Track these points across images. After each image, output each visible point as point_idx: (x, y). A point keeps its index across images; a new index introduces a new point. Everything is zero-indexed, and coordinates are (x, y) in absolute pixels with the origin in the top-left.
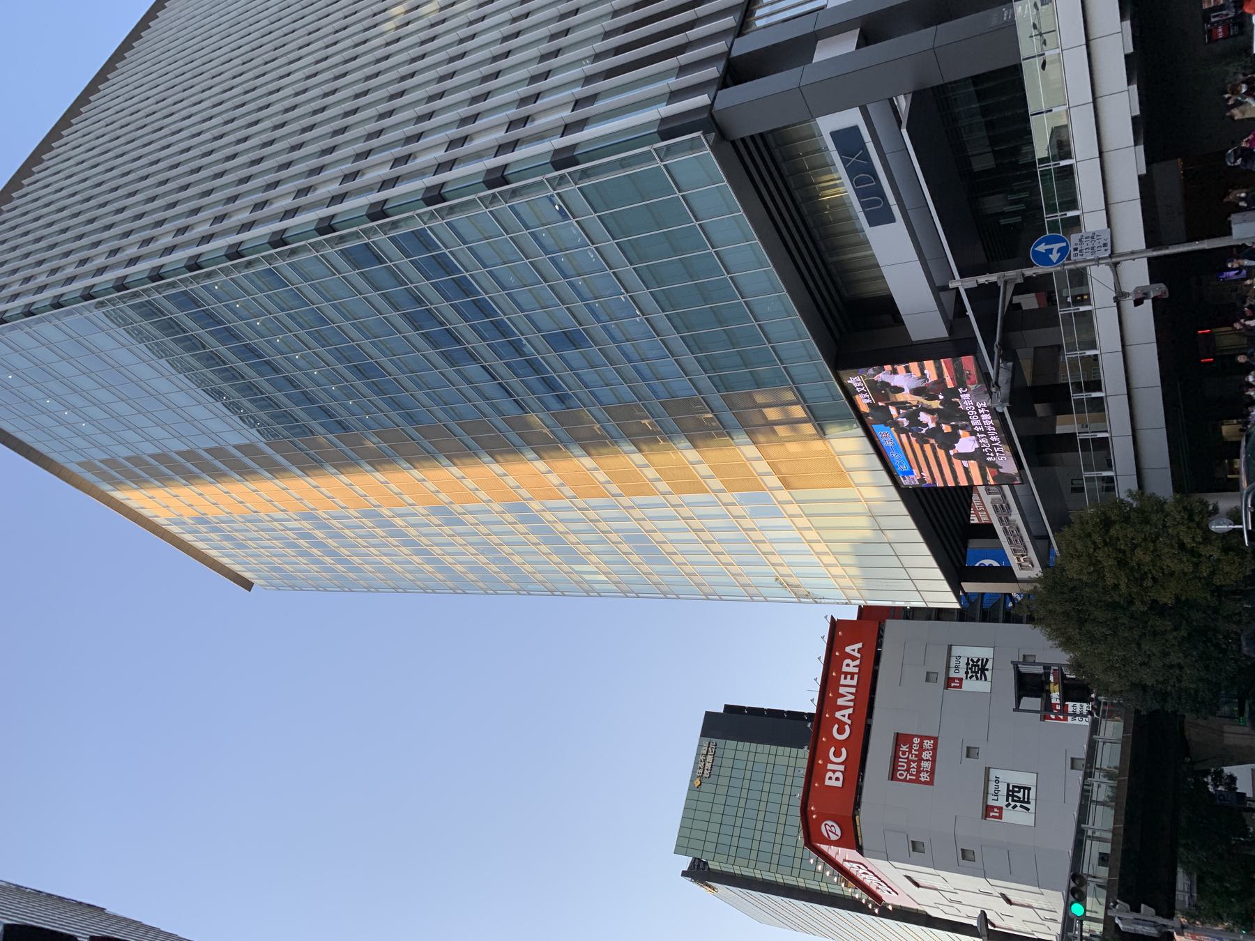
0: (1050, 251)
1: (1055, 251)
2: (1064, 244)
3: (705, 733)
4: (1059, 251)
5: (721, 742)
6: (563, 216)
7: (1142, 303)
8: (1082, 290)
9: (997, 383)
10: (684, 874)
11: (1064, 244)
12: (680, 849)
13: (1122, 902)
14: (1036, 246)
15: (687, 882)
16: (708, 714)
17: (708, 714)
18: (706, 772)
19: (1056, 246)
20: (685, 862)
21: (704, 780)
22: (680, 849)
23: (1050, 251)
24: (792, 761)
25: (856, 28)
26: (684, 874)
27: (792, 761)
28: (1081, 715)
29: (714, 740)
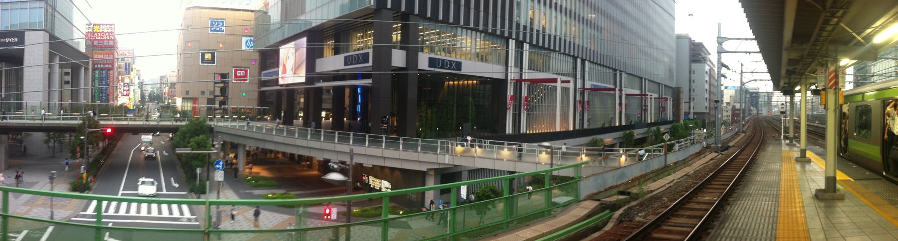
19: (220, 167)
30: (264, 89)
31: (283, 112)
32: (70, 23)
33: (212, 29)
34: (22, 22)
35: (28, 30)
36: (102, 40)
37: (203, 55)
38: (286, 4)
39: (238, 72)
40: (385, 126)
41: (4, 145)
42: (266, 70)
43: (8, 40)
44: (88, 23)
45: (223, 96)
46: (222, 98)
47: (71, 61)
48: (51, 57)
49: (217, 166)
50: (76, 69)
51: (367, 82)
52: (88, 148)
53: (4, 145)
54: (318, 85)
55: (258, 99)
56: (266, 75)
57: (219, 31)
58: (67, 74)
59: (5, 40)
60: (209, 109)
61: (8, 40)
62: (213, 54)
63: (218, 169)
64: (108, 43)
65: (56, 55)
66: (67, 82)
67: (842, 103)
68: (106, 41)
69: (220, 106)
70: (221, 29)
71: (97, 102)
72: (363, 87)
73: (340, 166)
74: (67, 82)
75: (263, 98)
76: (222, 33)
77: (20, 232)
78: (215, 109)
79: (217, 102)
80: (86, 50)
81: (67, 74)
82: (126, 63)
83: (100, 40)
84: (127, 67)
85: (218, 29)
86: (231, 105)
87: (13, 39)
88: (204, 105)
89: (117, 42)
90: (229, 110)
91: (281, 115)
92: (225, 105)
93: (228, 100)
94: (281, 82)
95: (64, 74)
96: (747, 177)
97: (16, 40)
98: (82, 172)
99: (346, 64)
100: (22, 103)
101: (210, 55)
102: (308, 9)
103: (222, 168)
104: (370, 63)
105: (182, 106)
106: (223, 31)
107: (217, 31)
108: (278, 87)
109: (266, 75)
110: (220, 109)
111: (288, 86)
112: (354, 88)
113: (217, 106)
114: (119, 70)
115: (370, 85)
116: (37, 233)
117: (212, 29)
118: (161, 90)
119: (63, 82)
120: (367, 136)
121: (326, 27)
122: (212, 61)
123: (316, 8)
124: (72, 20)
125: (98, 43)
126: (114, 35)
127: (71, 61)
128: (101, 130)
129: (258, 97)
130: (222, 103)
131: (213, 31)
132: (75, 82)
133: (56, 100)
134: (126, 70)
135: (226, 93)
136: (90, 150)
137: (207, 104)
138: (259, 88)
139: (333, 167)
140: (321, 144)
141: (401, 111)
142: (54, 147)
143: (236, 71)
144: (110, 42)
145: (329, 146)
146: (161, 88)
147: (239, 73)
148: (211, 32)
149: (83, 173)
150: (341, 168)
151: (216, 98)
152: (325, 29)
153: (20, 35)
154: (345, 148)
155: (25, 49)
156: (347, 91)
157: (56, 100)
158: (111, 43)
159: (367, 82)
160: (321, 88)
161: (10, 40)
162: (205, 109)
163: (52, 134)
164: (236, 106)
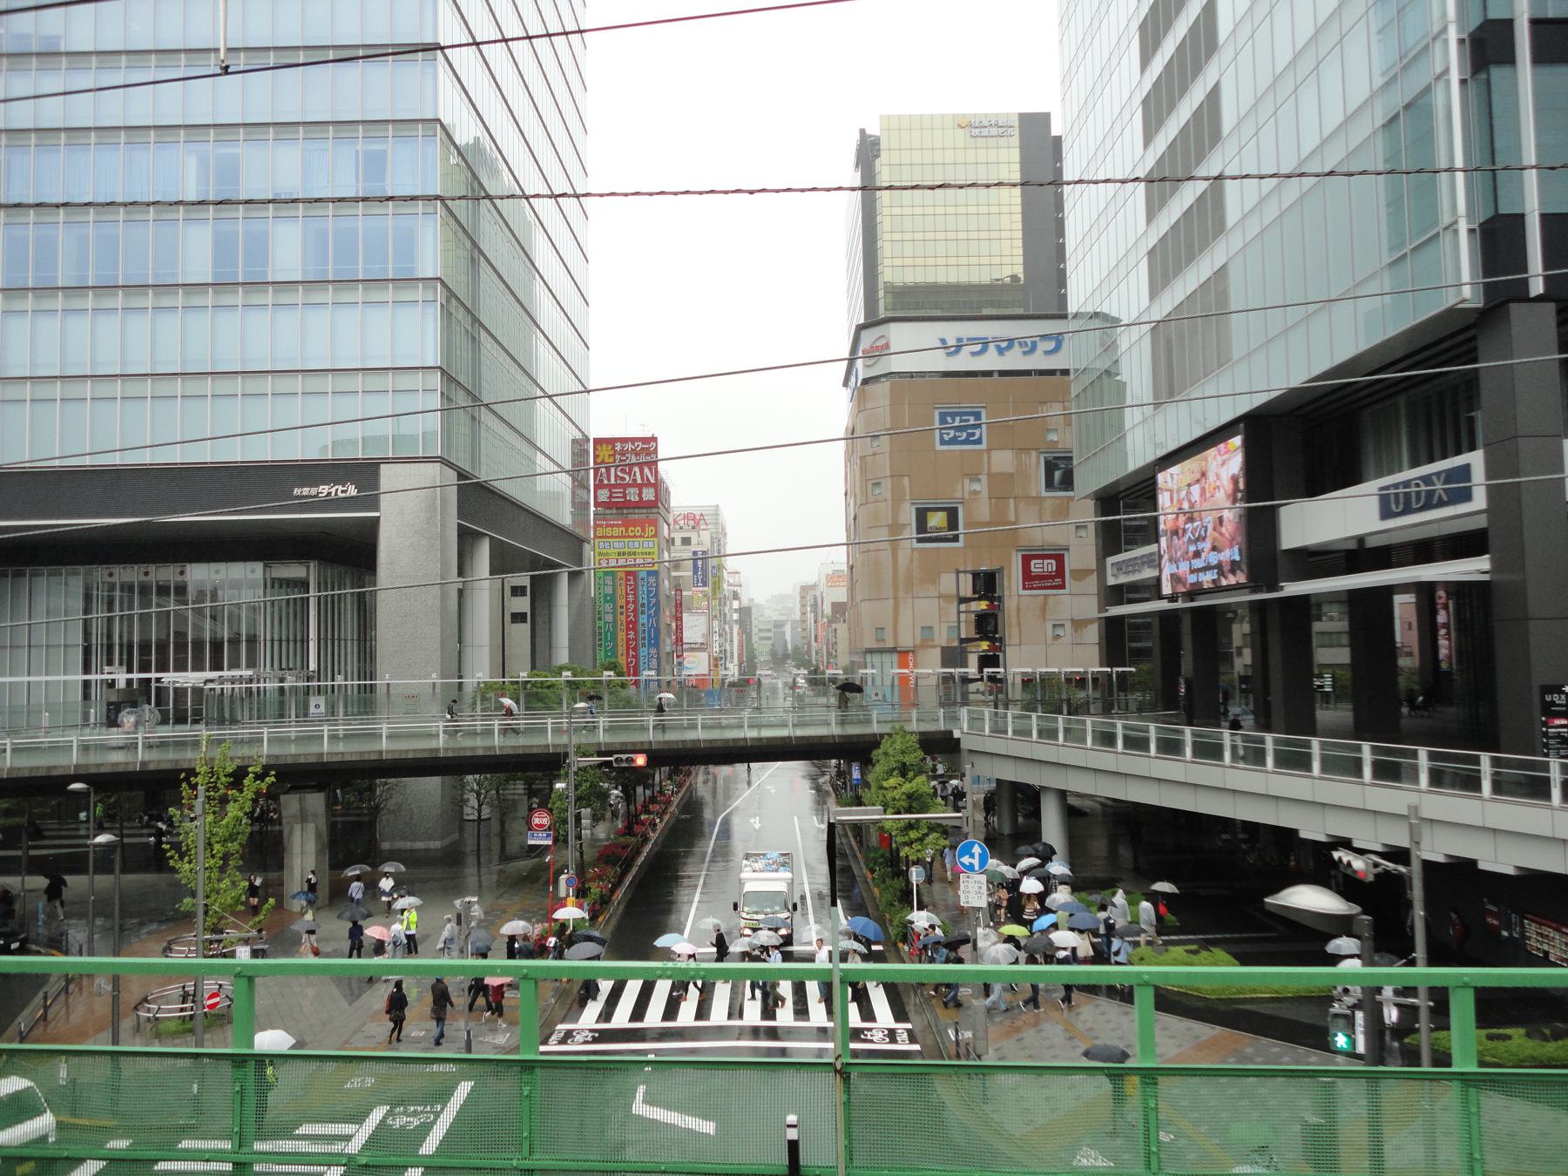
0: (972, 856)
1: (971, 860)
2: (977, 868)
3: (1024, 118)
4: (971, 864)
5: (1015, 141)
8: (1448, 779)
10: (862, 132)
11: (977, 868)
12: (886, 120)
13: (1136, 1025)
16: (832, 603)
17: (832, 603)
19: (976, 862)
20: (873, 130)
21: (968, 130)
23: (972, 856)
25: (609, 979)
26: (862, 132)
28: (906, 844)
30: (1116, 611)
31: (1182, 681)
35: (388, 461)
38: (1169, 341)
40: (1558, 722)
41: (311, 826)
45: (988, 639)
48: (467, 538)
49: (966, 860)
51: (1472, 568)
52: (578, 818)
53: (311, 826)
54: (1292, 589)
56: (1119, 566)
58: (518, 591)
59: (314, 491)
60: (947, 679)
61: (324, 489)
62: (952, 515)
63: (971, 867)
64: (640, 494)
66: (518, 618)
68: (632, 490)
69: (981, 671)
70: (973, 434)
71: (606, 673)
72: (1459, 590)
73: (1376, 865)
74: (518, 618)
75: (1116, 638)
76: (977, 447)
77: (358, 1118)
78: (966, 680)
79: (973, 660)
81: (518, 591)
83: (616, 486)
86: (1018, 664)
87: (341, 488)
88: (239, 403)
89: (667, 489)
93: (1005, 653)
97: (352, 491)
99: (1386, 514)
104: (1479, 501)
106: (979, 441)
107: (962, 443)
108: (1163, 605)
109: (1119, 566)
110: (981, 679)
112: (1425, 591)
113: (972, 670)
114: (673, 574)
115: (1486, 578)
116: (415, 1113)
118: (804, 630)
119: (508, 618)
120: (874, 671)
123: (1286, 331)
125: (610, 497)
126: (655, 463)
129: (1100, 638)
130: (987, 661)
131: (953, 441)
133: (480, 675)
134: (695, 572)
136: (585, 822)
138: (1101, 609)
139: (1349, 864)
140: (1312, 785)
141: (319, 693)
145: (1340, 790)
147: (1036, 567)
148: (945, 448)
150: (1379, 870)
151: (971, 647)
153: (365, 472)
154: (1392, 798)
155: (381, 519)
156: (1403, 605)
158: (648, 494)
159: (1472, 568)
160: (1304, 600)
161: (333, 490)
163: (470, 778)
164: (1030, 670)
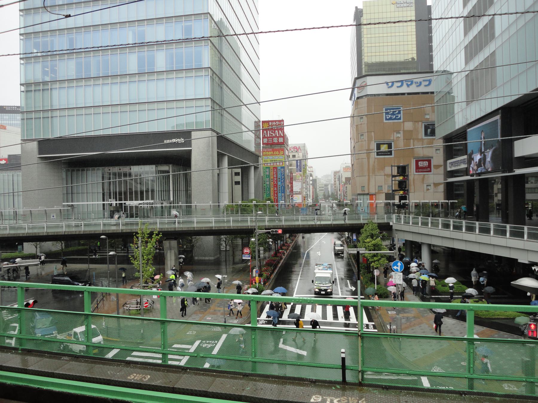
0: (398, 266)
1: (397, 268)
2: (399, 270)
4: (397, 269)
6: (179, 361)
7: (435, 322)
9: (119, 208)
10: (356, 8)
11: (399, 270)
14: (400, 262)
15: (354, 10)
16: (345, 178)
17: (345, 178)
18: (399, 5)
19: (399, 268)
20: (360, 7)
21: (395, 5)
22: (365, 3)
23: (398, 266)
24: (410, 33)
26: (356, 8)
27: (410, 33)
29: (414, 5)
32: (239, 122)
33: (388, 118)
34: (187, 122)
35: (194, 130)
36: (271, 137)
37: (378, 146)
38: (472, 81)
39: (419, 162)
41: (173, 251)
42: (452, 158)
43: (174, 140)
44: (257, 120)
46: (401, 192)
47: (249, 164)
48: (220, 156)
49: (395, 267)
50: (245, 171)
53: (173, 251)
54: (518, 171)
55: (444, 191)
56: (452, 164)
57: (395, 119)
58: (237, 174)
61: (174, 140)
62: (390, 146)
63: (397, 270)
64: (278, 140)
65: (226, 155)
66: (237, 183)
67: (496, 192)
70: (398, 116)
74: (237, 183)
79: (397, 198)
80: (255, 150)
82: (297, 161)
83: (269, 137)
84: (299, 164)
85: (394, 117)
86: (413, 199)
90: (411, 205)
91: (473, 209)
92: (406, 200)
94: (24, 253)
95: (233, 174)
96: (497, 215)
98: (254, 275)
100: (190, 207)
101: (386, 146)
102: (499, 83)
103: (400, 270)
105: (62, 174)
106: (400, 119)
109: (452, 164)
111: (480, 176)
113: (397, 201)
114: (290, 168)
117: (388, 118)
118: (335, 187)
119: (234, 183)
121: (454, 135)
122: (390, 153)
123: (504, 84)
124: (241, 118)
125: (268, 141)
127: (249, 164)
128: (272, 231)
129: (444, 190)
131: (390, 119)
132: (244, 183)
133: (226, 202)
135: (406, 187)
136: (261, 252)
137: (386, 200)
138: (445, 179)
142: (226, 250)
143: (417, 162)
144: (280, 139)
146: (335, 184)
147: (421, 164)
149: (255, 277)
151: (396, 193)
152: (454, 136)
153: (187, 134)
157: (226, 202)
158: (281, 140)
160: (523, 176)
161: (177, 141)
162: (383, 205)
